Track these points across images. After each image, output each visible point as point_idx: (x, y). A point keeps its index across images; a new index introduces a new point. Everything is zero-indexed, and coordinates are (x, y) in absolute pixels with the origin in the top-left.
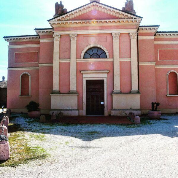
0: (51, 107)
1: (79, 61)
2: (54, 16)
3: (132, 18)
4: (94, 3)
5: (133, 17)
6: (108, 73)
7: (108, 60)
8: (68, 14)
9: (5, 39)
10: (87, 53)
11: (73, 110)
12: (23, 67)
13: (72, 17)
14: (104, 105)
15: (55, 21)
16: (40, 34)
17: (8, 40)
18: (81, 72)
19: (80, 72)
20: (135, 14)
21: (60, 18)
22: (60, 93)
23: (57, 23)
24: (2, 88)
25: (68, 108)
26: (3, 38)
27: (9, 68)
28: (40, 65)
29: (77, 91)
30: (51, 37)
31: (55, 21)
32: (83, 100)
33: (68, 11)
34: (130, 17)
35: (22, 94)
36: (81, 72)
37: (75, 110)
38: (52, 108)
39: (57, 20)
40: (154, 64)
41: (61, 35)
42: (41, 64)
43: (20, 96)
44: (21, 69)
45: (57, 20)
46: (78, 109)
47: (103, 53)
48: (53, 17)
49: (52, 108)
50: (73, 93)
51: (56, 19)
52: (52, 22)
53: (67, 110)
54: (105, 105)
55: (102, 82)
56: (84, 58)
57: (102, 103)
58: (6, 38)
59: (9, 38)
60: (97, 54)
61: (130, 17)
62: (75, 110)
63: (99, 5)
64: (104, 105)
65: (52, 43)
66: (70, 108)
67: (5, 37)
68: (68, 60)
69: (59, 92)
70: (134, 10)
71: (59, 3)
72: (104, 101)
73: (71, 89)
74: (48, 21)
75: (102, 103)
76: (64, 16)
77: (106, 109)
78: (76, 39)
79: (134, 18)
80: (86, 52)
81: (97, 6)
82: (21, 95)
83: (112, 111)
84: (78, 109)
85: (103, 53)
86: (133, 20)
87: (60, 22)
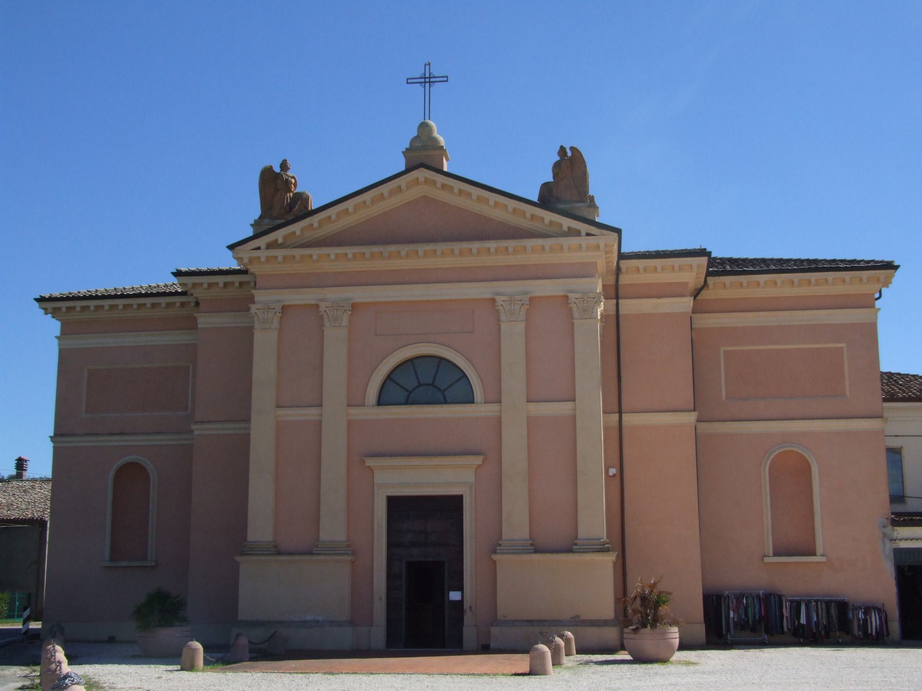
0: (671, 657)
1: (357, 413)
2: (256, 224)
3: (578, 233)
4: (422, 174)
5: (583, 227)
6: (479, 466)
7: (479, 410)
8: (315, 219)
9: (45, 309)
10: (391, 380)
11: (332, 623)
12: (122, 434)
13: (329, 229)
14: (460, 603)
15: (259, 248)
16: (198, 293)
17: (55, 313)
18: (367, 464)
19: (364, 462)
20: (586, 214)
21: (279, 235)
22: (279, 553)
23: (268, 258)
24: (17, 521)
25: (309, 618)
26: (36, 304)
27: (59, 439)
28: (197, 429)
29: (348, 546)
30: (243, 304)
31: (259, 248)
32: (372, 583)
33: (314, 204)
34: (569, 228)
35: (116, 553)
36: (367, 464)
37: (339, 624)
38: (240, 617)
39: (269, 246)
40: (692, 417)
41: (284, 308)
42: (202, 422)
43: (109, 564)
44: (115, 441)
45: (269, 246)
46: (352, 623)
47: (459, 379)
48: (250, 232)
49: (240, 617)
50: (333, 550)
51: (262, 242)
52: (246, 252)
53: (304, 624)
54: (466, 605)
55: (453, 505)
56: (380, 402)
57: (455, 596)
58: (50, 305)
59: (64, 305)
60: (432, 385)
61: (569, 228)
62: (339, 624)
63: (440, 179)
64: (460, 603)
65: (248, 333)
66: (320, 618)
67: (41, 300)
68: (311, 414)
69: (275, 547)
70: (591, 192)
71: (277, 169)
72: (460, 588)
73: (323, 536)
74: (231, 247)
75: (455, 596)
76: (296, 228)
77: (468, 618)
78: (345, 322)
79: (588, 235)
80: (389, 378)
81: (435, 182)
82: (112, 559)
83: (495, 631)
84: (352, 623)
85: (459, 379)
86: (584, 241)
87: (280, 253)
